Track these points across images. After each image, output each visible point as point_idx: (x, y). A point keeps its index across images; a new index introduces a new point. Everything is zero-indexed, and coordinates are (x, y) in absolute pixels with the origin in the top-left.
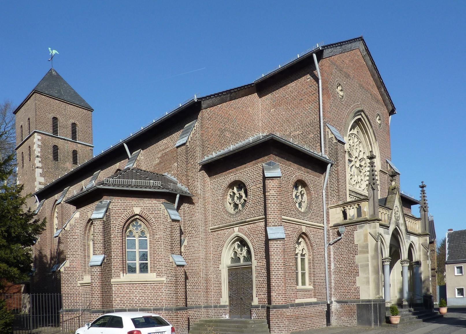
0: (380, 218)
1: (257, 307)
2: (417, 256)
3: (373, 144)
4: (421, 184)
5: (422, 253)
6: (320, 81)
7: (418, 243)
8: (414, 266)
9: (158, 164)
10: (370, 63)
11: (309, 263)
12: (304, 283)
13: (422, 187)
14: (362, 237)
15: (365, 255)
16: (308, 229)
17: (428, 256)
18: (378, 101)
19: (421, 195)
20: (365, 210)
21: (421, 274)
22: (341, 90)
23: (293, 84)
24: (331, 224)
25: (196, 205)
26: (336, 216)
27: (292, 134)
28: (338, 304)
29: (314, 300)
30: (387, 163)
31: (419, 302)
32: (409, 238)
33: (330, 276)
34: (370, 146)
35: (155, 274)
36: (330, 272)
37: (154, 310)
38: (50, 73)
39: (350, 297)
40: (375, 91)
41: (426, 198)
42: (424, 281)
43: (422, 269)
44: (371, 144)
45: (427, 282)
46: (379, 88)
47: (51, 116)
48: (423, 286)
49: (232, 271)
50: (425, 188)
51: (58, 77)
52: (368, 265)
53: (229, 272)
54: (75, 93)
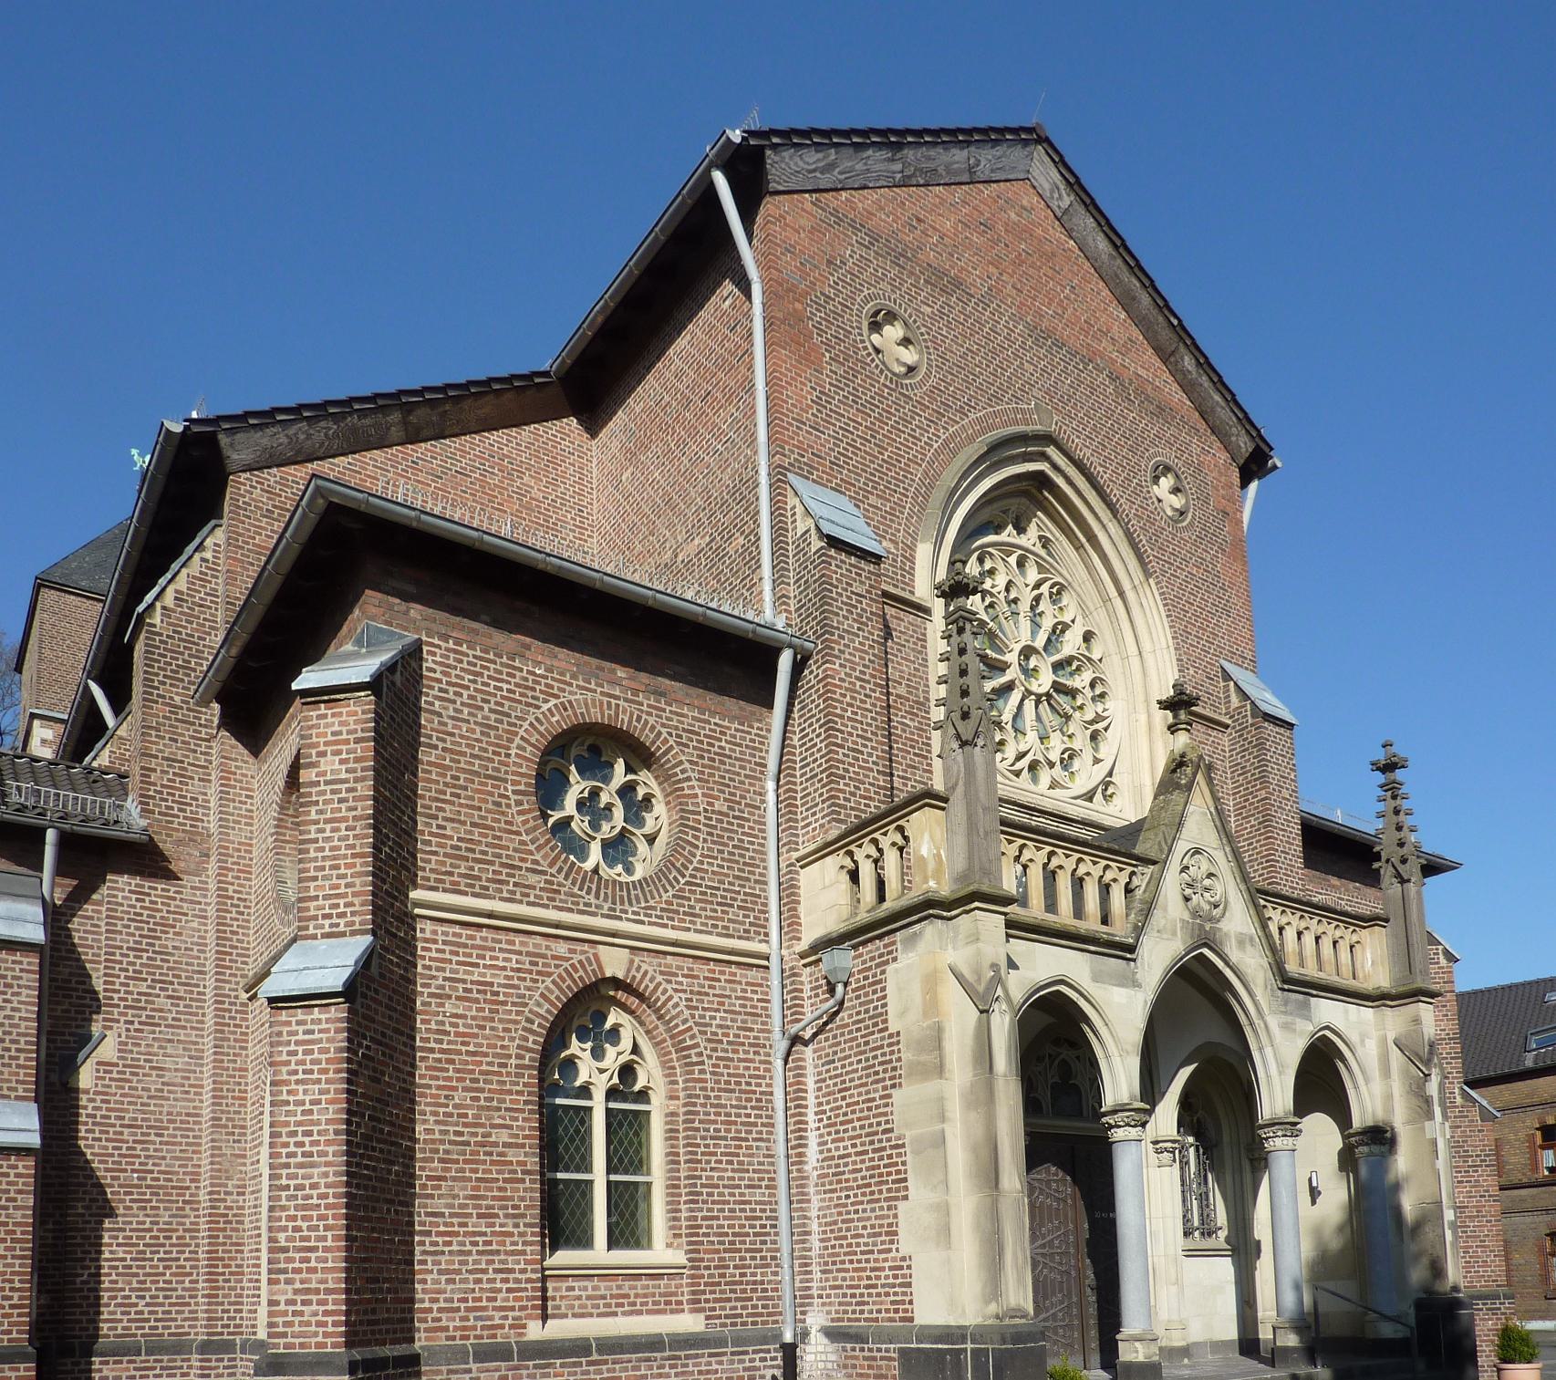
0: (1009, 885)
2: (1374, 1093)
3: (1130, 595)
4: (1381, 756)
5: (1398, 1088)
6: (756, 289)
7: (1375, 1034)
8: (1369, 1147)
10: (1102, 245)
11: (671, 1135)
12: (627, 1231)
13: (1389, 767)
14: (916, 989)
15: (930, 1087)
16: (648, 965)
17: (1428, 1101)
18: (1163, 411)
19: (1381, 807)
20: (924, 851)
21: (1397, 1187)
22: (906, 342)
23: (682, 342)
24: (808, 936)
25: (187, 881)
26: (826, 898)
27: (680, 558)
28: (832, 1347)
29: (689, 1323)
30: (1227, 677)
31: (1388, 1330)
32: (1305, 1012)
33: (798, 1199)
34: (1118, 602)
36: (798, 1182)
39: (876, 1310)
40: (1146, 365)
41: (1408, 821)
42: (1418, 1226)
43: (1402, 1162)
44: (1121, 594)
45: (1429, 1233)
46: (1166, 356)
48: (1413, 1248)
50: (1399, 774)
52: (941, 1141)
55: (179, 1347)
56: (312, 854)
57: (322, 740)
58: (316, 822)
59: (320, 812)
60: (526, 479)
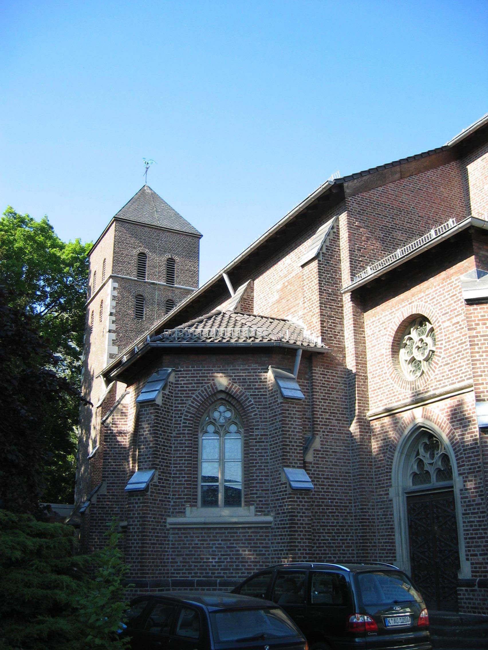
1: (469, 583)
9: (278, 302)
35: (252, 508)
37: (221, 584)
38: (142, 191)
47: (135, 252)
49: (413, 500)
51: (154, 195)
53: (408, 504)
54: (177, 214)
55: (214, 584)
56: (478, 366)
57: (477, 319)
58: (478, 352)
59: (480, 348)
60: (441, 189)
